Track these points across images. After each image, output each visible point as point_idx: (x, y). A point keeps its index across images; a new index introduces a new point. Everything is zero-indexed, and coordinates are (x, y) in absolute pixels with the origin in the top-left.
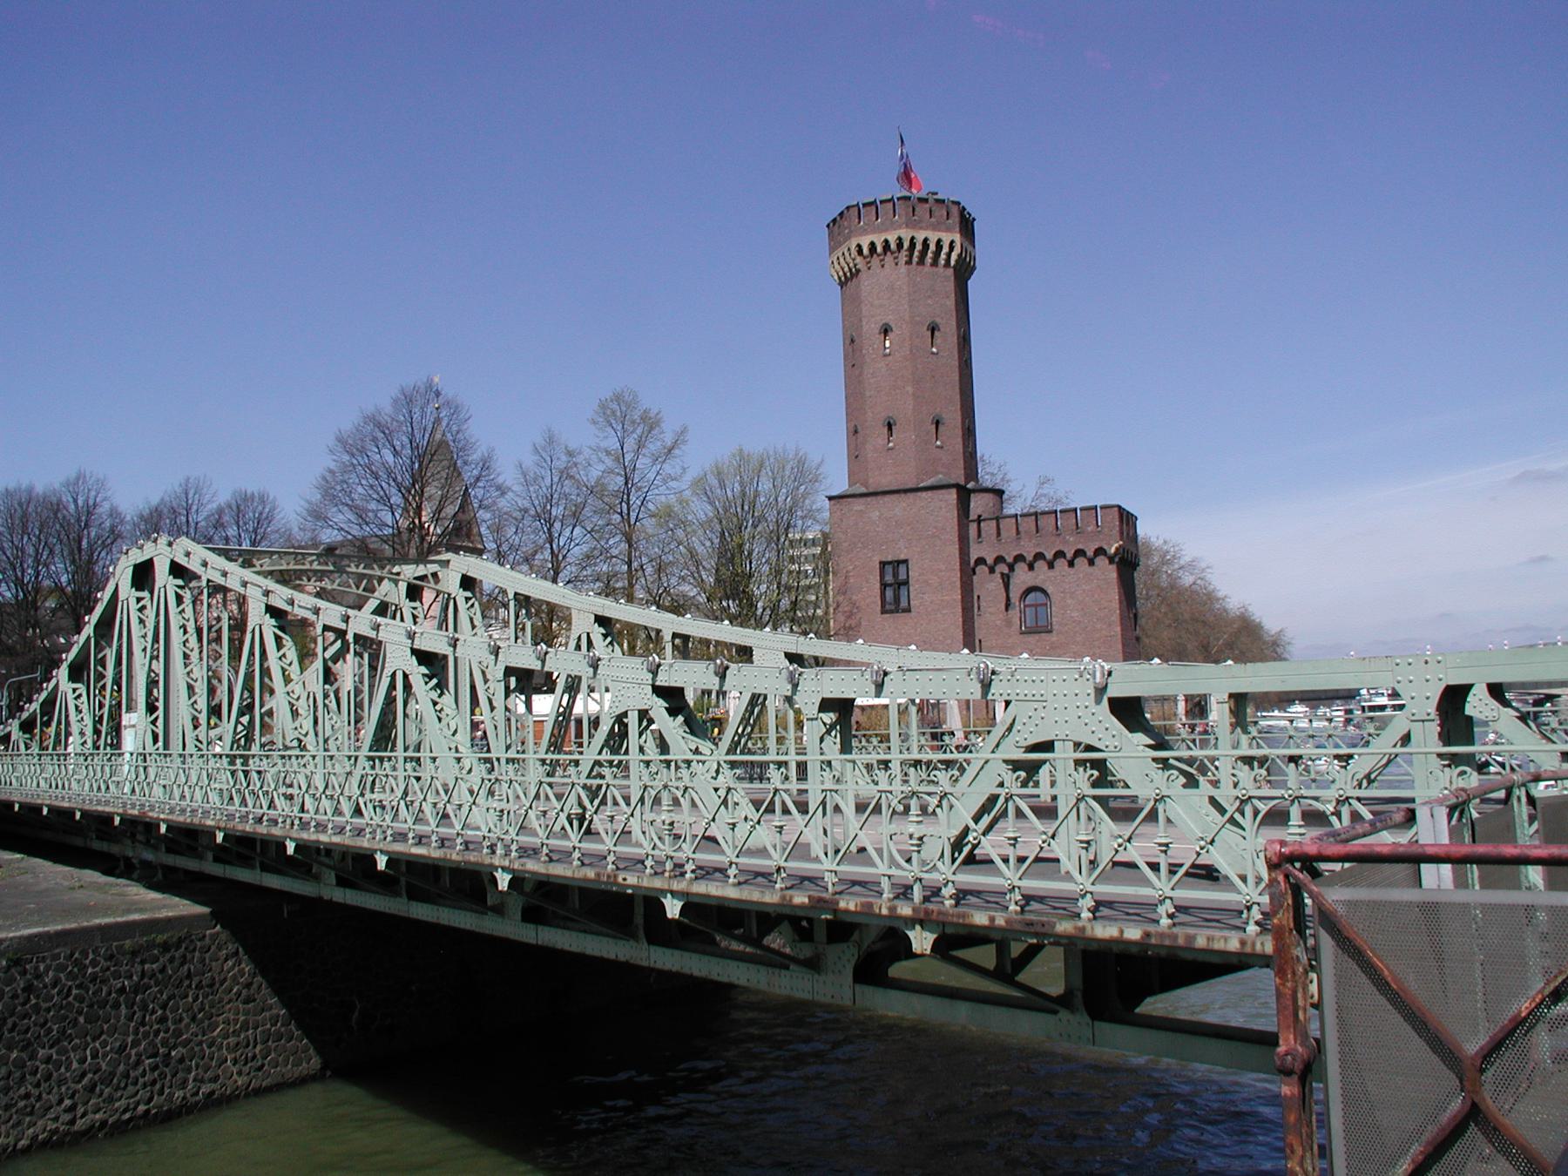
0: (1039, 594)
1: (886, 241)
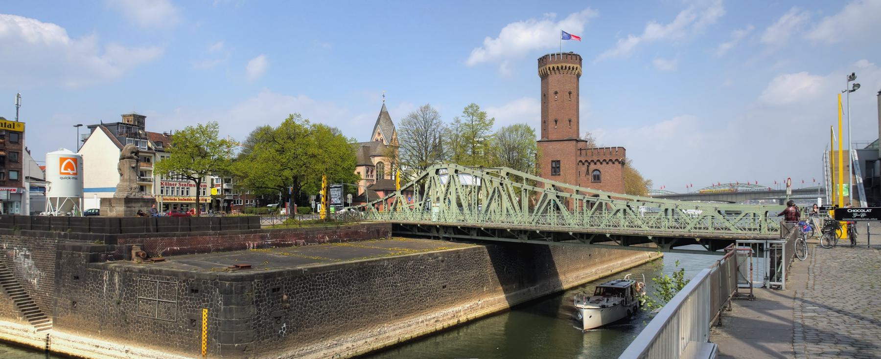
1: (558, 67)
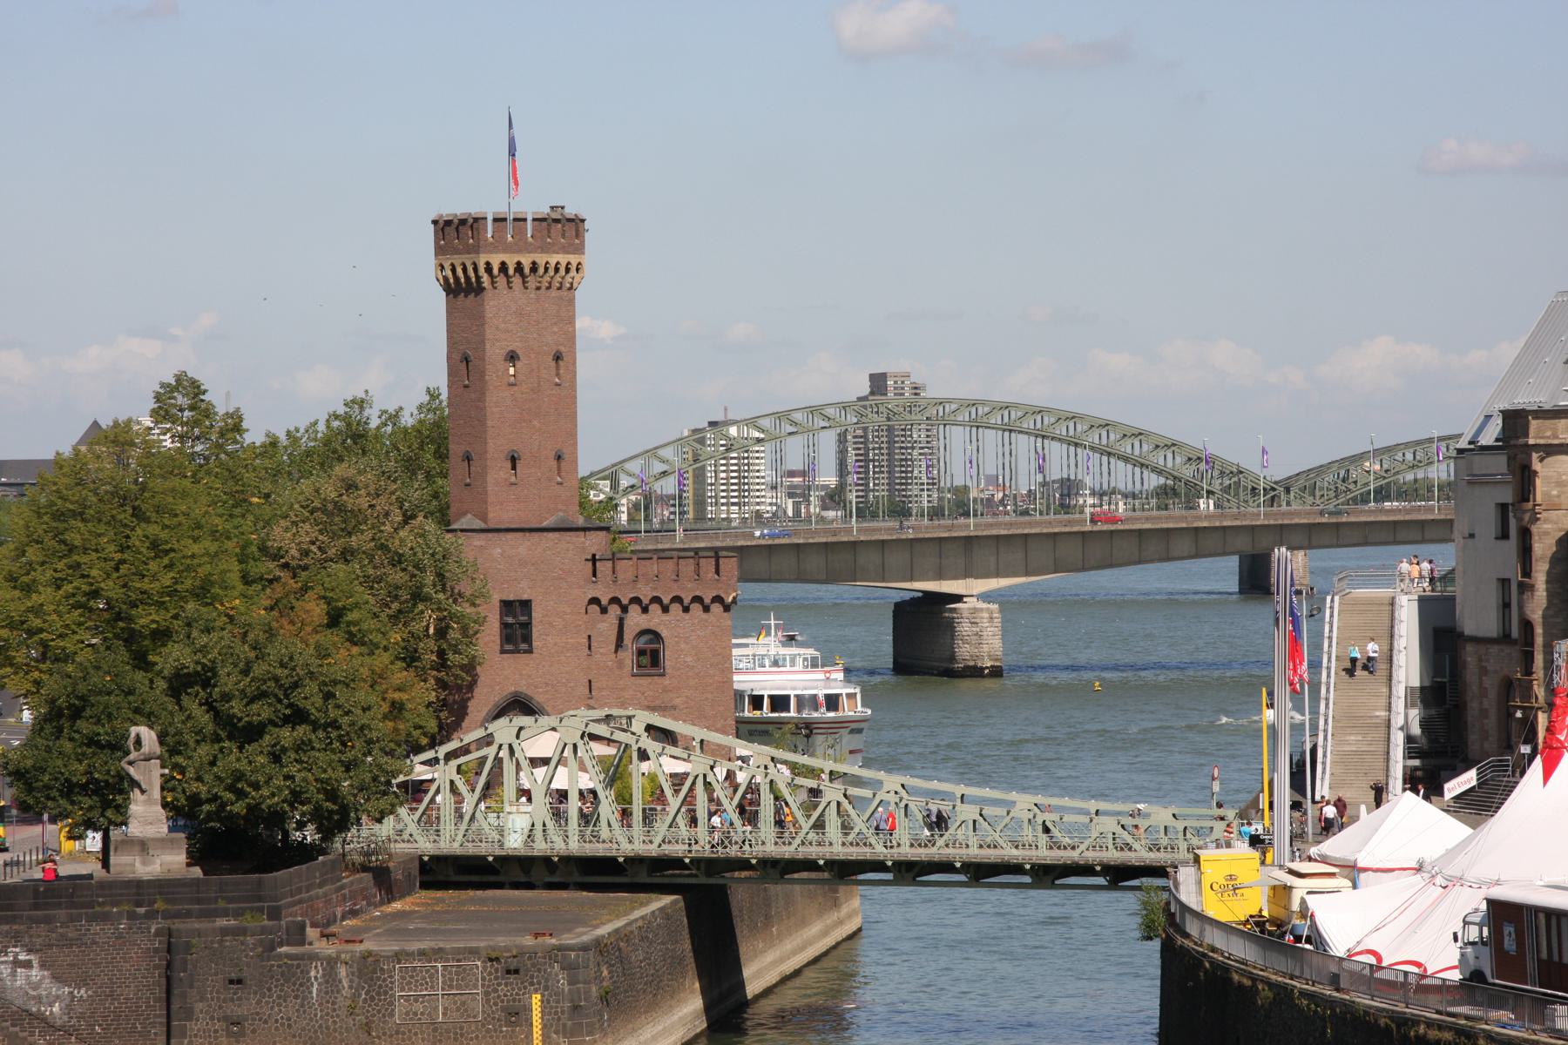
1: (519, 263)
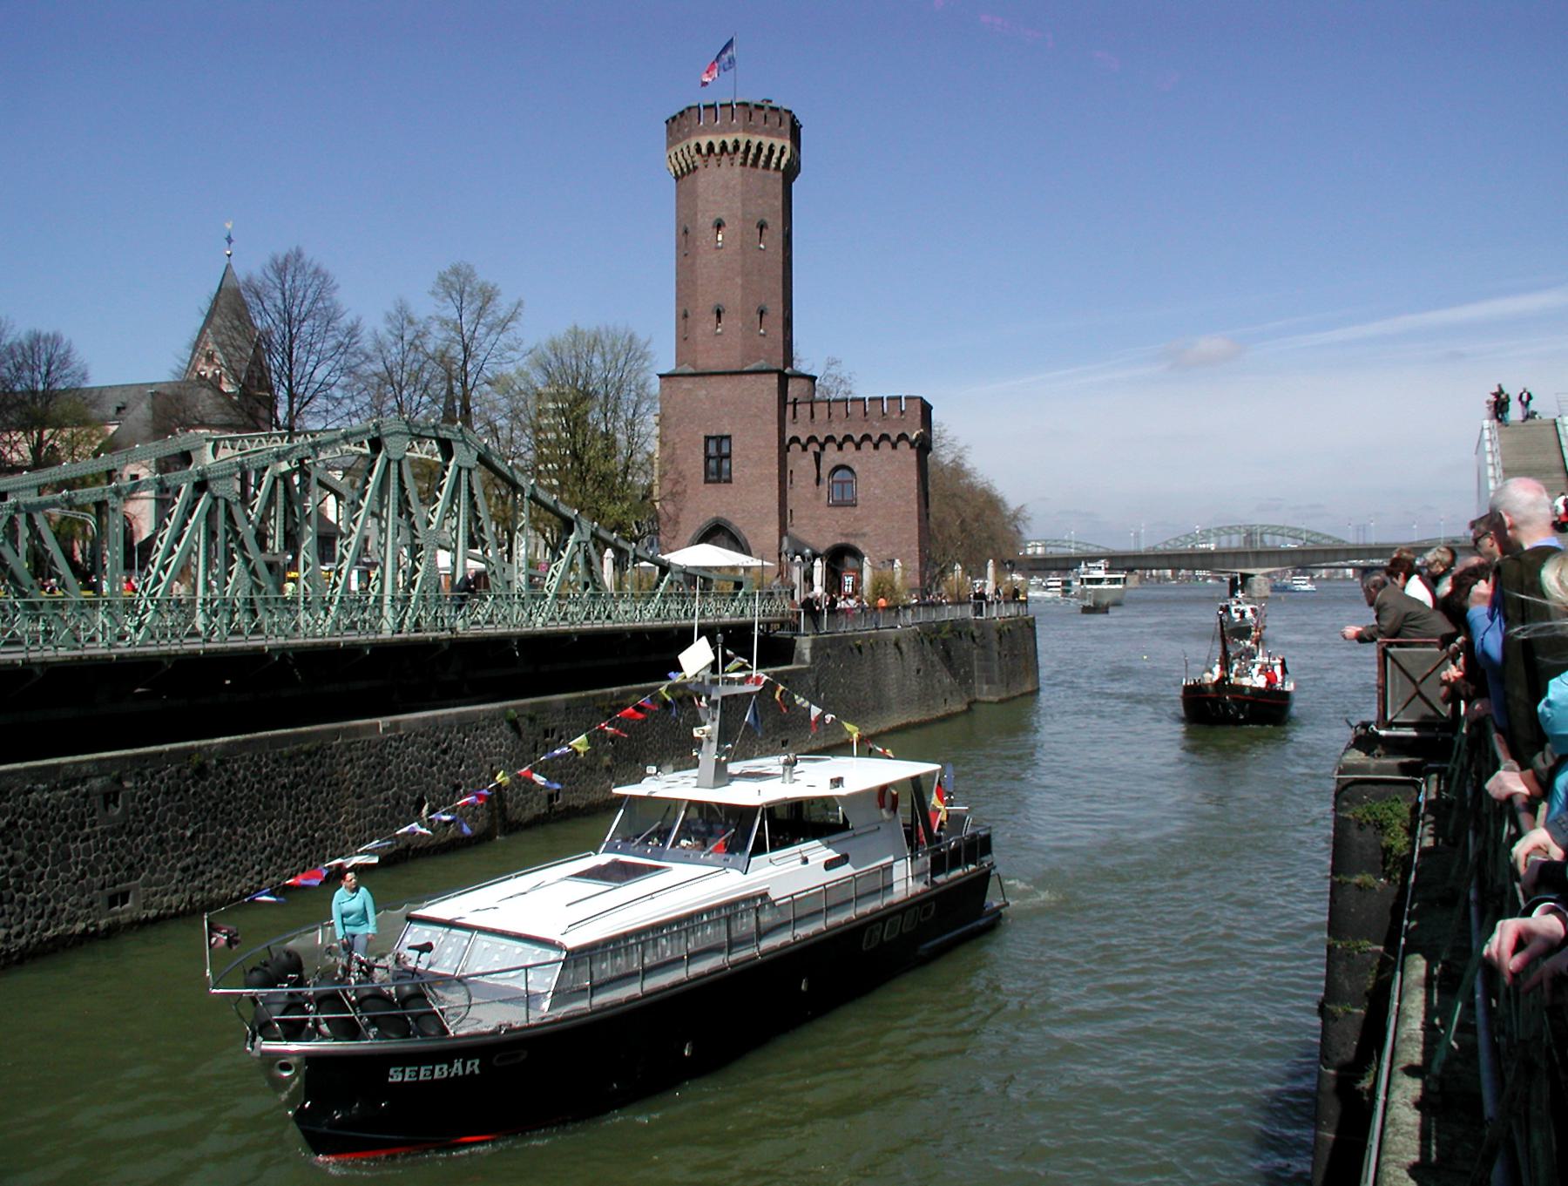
0: (847, 473)
1: (724, 143)
